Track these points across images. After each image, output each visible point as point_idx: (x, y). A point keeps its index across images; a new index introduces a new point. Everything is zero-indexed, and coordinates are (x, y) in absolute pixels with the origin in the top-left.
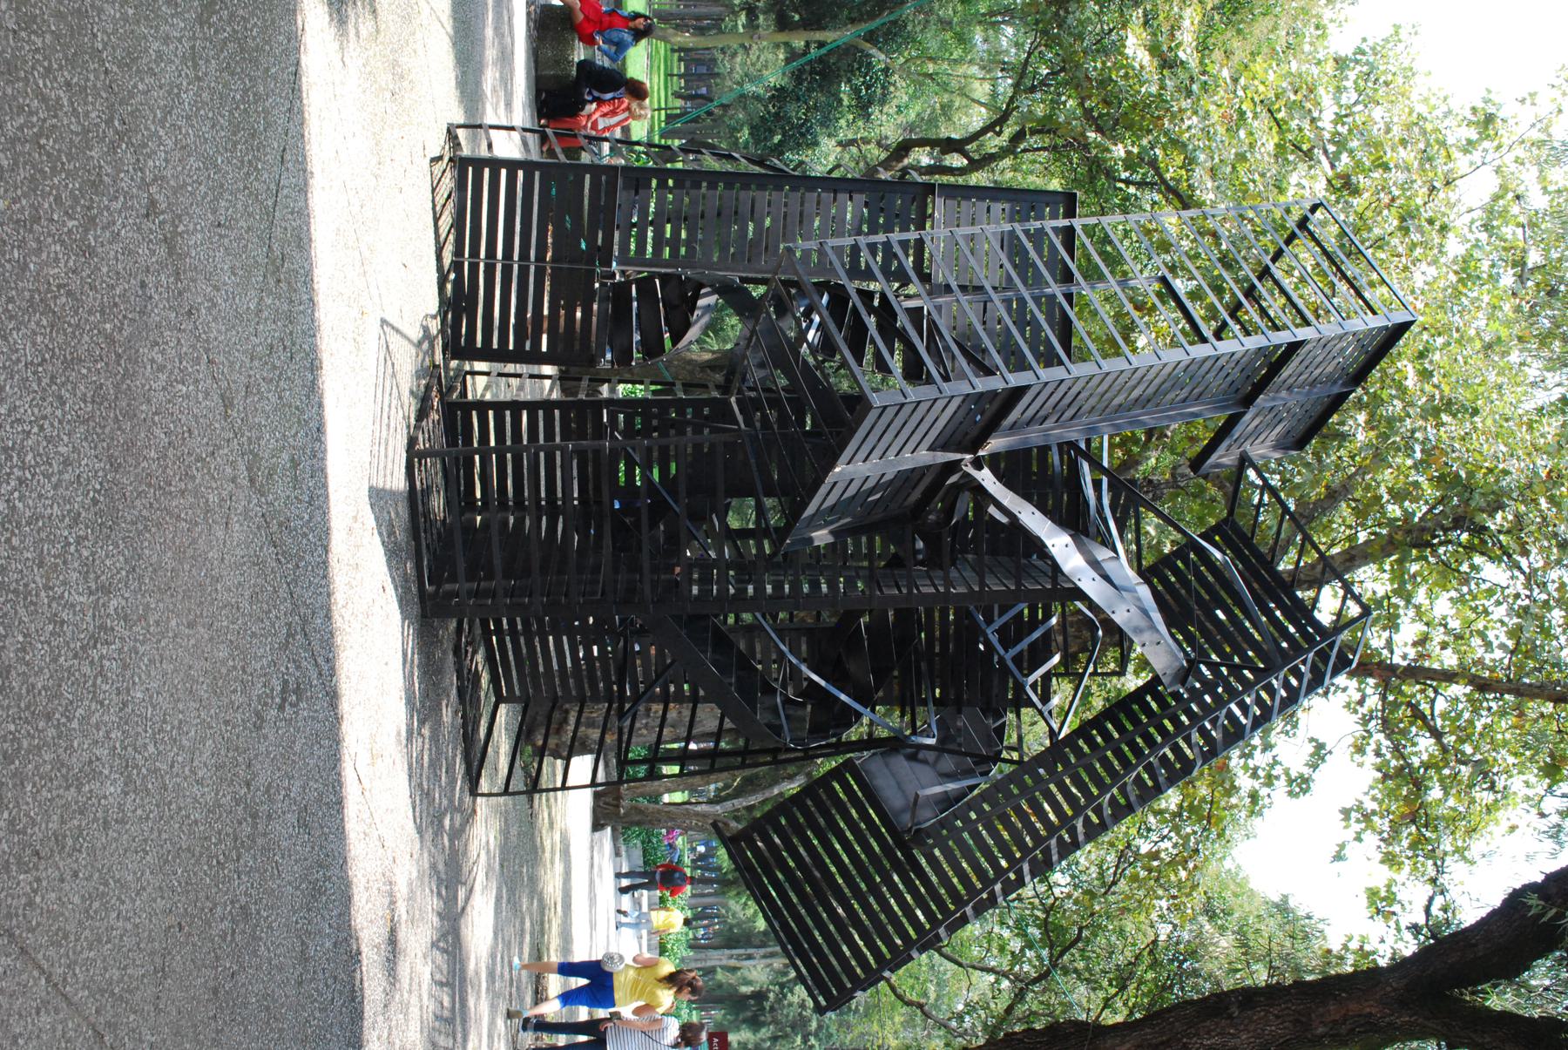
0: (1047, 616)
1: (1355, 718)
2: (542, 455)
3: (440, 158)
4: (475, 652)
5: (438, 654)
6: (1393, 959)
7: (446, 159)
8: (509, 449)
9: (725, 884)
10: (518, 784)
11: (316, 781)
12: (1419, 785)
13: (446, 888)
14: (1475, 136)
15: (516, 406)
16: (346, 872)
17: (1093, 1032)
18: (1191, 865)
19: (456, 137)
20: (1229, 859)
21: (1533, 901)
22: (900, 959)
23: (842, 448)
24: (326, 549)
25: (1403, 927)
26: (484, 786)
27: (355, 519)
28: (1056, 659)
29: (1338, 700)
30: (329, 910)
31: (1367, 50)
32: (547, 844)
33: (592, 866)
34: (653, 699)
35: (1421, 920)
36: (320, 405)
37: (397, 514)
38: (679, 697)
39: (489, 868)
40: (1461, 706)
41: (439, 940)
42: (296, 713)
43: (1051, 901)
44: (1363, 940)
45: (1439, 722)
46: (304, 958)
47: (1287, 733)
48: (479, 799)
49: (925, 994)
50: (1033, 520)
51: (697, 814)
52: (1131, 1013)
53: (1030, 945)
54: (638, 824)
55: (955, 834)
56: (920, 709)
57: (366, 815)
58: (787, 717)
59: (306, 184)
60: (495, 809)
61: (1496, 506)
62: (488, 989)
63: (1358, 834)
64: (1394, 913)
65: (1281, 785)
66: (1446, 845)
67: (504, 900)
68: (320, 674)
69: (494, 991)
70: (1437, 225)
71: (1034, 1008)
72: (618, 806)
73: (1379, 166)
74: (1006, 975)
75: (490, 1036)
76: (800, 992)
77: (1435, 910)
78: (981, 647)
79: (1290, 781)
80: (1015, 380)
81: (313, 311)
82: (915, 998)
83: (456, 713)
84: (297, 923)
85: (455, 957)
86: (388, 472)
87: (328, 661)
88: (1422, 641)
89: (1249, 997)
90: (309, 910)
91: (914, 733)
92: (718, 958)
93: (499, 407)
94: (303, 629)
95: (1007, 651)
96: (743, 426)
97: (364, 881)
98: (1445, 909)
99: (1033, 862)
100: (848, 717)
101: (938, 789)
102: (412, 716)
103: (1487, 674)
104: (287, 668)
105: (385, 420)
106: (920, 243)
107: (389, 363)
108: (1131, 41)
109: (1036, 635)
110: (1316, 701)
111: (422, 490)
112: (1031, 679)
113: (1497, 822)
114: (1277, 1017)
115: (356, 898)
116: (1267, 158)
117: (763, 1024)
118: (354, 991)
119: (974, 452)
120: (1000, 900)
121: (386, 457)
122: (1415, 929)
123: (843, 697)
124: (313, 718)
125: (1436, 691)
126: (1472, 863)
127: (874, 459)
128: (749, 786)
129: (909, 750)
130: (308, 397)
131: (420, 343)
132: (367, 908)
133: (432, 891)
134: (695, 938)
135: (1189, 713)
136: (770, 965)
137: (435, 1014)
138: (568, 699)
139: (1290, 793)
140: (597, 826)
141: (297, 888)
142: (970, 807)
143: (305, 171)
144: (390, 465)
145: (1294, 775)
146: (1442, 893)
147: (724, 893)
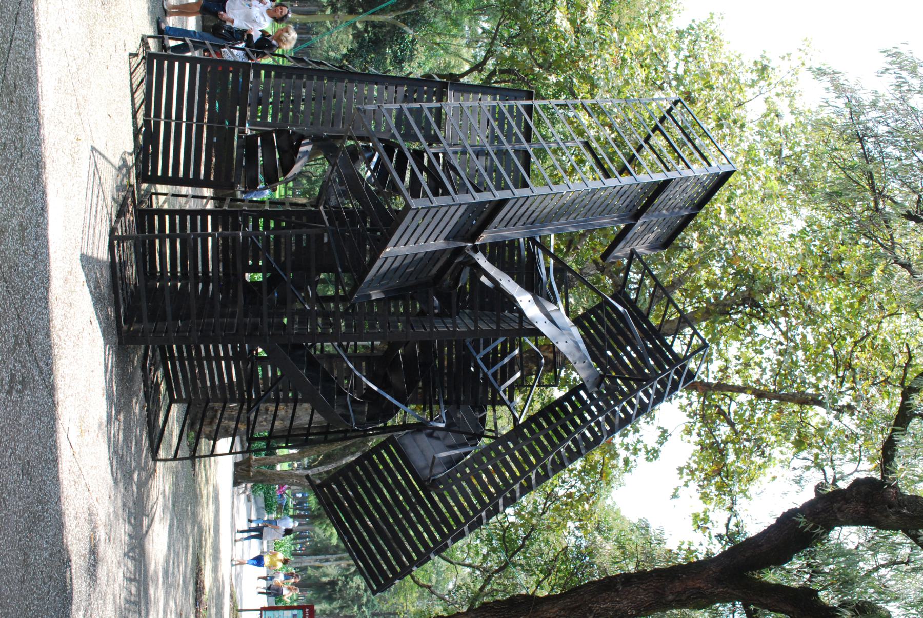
0: (513, 350)
1: (685, 414)
2: (199, 240)
3: (136, 55)
4: (156, 371)
5: (130, 369)
6: (707, 554)
7: (141, 57)
8: (179, 236)
9: (314, 517)
10: (184, 452)
11: (37, 444)
12: (723, 453)
13: (135, 518)
14: (756, 78)
15: (183, 213)
16: (60, 507)
17: (530, 600)
18: (591, 502)
19: (147, 43)
20: (609, 498)
21: (802, 519)
22: (423, 559)
23: (391, 235)
24: (47, 290)
25: (713, 536)
26: (162, 454)
27: (70, 273)
28: (518, 375)
29: (676, 402)
30: (46, 532)
31: (695, 26)
32: (204, 493)
33: (233, 508)
34: (269, 400)
35: (724, 532)
36: (44, 193)
37: (102, 275)
38: (286, 400)
39: (165, 506)
40: (744, 408)
41: (129, 552)
42: (22, 398)
43: (507, 524)
44: (690, 544)
45: (732, 416)
46: (25, 564)
47: (648, 423)
48: (158, 463)
49: (430, 580)
50: (510, 285)
51: (297, 476)
52: (552, 589)
53: (494, 550)
54: (262, 482)
55: (457, 482)
56: (435, 407)
57: (76, 469)
58: (354, 411)
59: (35, 42)
60: (170, 470)
61: (769, 289)
62: (163, 582)
63: (686, 482)
64: (708, 528)
65: (642, 454)
66: (736, 489)
67: (175, 527)
68: (41, 373)
69: (167, 583)
70: (739, 124)
71: (495, 587)
72: (249, 471)
73: (707, 87)
74: (478, 568)
75: (165, 612)
76: (358, 581)
77: (731, 526)
78: (472, 369)
79: (647, 452)
80: (500, 195)
81: (39, 129)
82: (425, 582)
83: (143, 407)
84: (20, 540)
85: (140, 562)
86: (95, 247)
87: (47, 364)
88: (724, 370)
89: (627, 578)
90: (30, 532)
91: (432, 420)
92: (308, 561)
93: (172, 213)
94: (28, 341)
95: (488, 369)
96: (327, 224)
97: (73, 512)
98: (737, 525)
99: (505, 498)
100: (391, 411)
101: (443, 455)
102: (111, 408)
103: (762, 388)
104: (14, 366)
105: (93, 213)
106: (439, 109)
107: (97, 176)
108: (558, 15)
109: (506, 360)
110: (664, 406)
111: (120, 263)
112: (503, 387)
113: (764, 475)
114: (645, 590)
115: (67, 524)
116: (641, 83)
117: (335, 599)
118: (66, 586)
119: (473, 242)
120: (484, 521)
121: (94, 236)
122: (720, 537)
123: (388, 397)
124: (35, 402)
125: (731, 399)
126: (750, 498)
127: (411, 244)
128: (329, 458)
129: (428, 431)
130: (34, 185)
131: (120, 169)
132: (76, 531)
133: (124, 520)
134: (296, 550)
135: (591, 413)
136: (339, 565)
137: (126, 599)
138: (216, 400)
139: (647, 459)
140: (236, 483)
141: (20, 517)
142: (466, 465)
143: (34, 33)
144: (96, 242)
145: (649, 448)
146: (735, 516)
147: (313, 523)
